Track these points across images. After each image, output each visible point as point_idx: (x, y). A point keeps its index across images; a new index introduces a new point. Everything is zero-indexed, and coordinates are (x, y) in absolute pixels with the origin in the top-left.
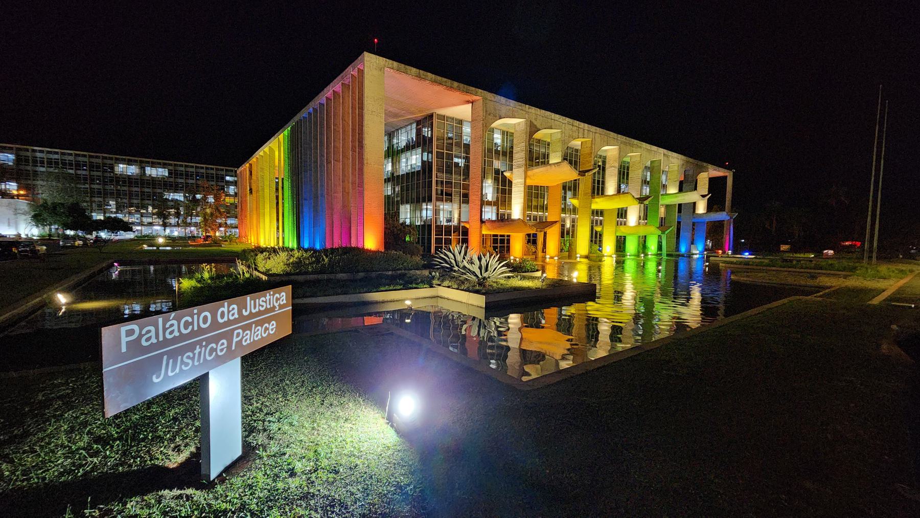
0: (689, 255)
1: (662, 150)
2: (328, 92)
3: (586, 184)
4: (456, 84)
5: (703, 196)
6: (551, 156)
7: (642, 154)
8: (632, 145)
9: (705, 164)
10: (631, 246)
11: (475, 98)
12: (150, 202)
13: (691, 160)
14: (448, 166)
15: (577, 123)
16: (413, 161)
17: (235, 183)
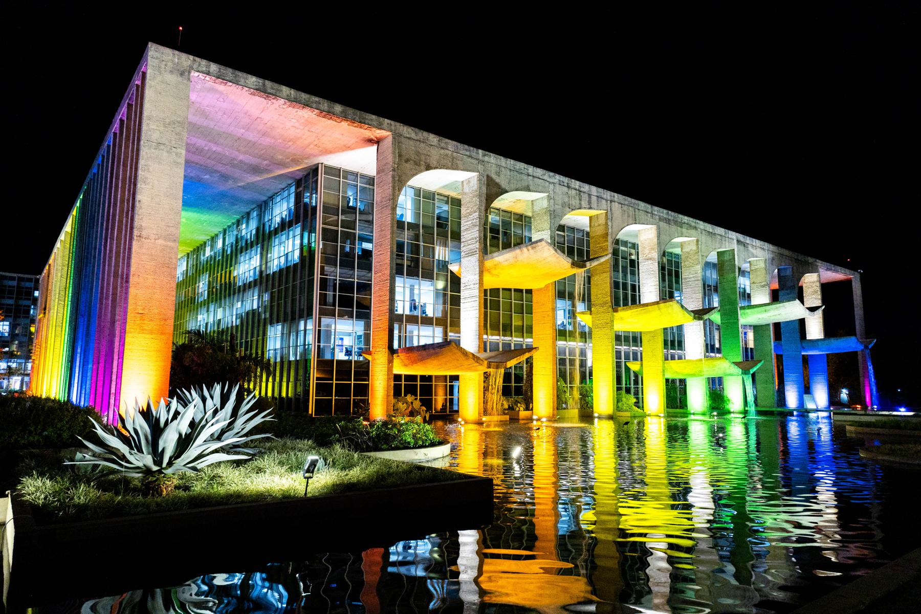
0: (803, 413)
1: (733, 235)
3: (602, 287)
4: (338, 108)
5: (812, 309)
7: (698, 243)
9: (811, 260)
10: (697, 398)
13: (786, 252)
14: (344, 255)
15: (576, 184)
16: (286, 250)
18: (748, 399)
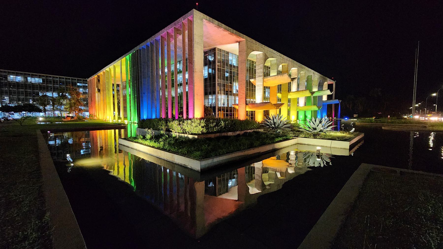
1: (312, 71)
2: (163, 32)
4: (235, 31)
6: (271, 71)
8: (302, 68)
11: (242, 39)
12: (31, 97)
17: (85, 87)
18: (171, 109)
